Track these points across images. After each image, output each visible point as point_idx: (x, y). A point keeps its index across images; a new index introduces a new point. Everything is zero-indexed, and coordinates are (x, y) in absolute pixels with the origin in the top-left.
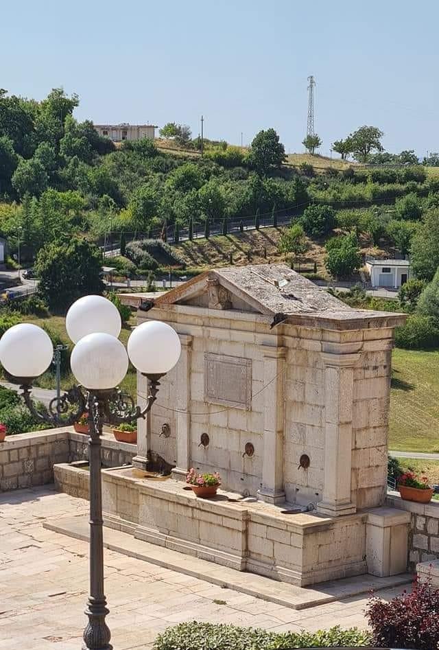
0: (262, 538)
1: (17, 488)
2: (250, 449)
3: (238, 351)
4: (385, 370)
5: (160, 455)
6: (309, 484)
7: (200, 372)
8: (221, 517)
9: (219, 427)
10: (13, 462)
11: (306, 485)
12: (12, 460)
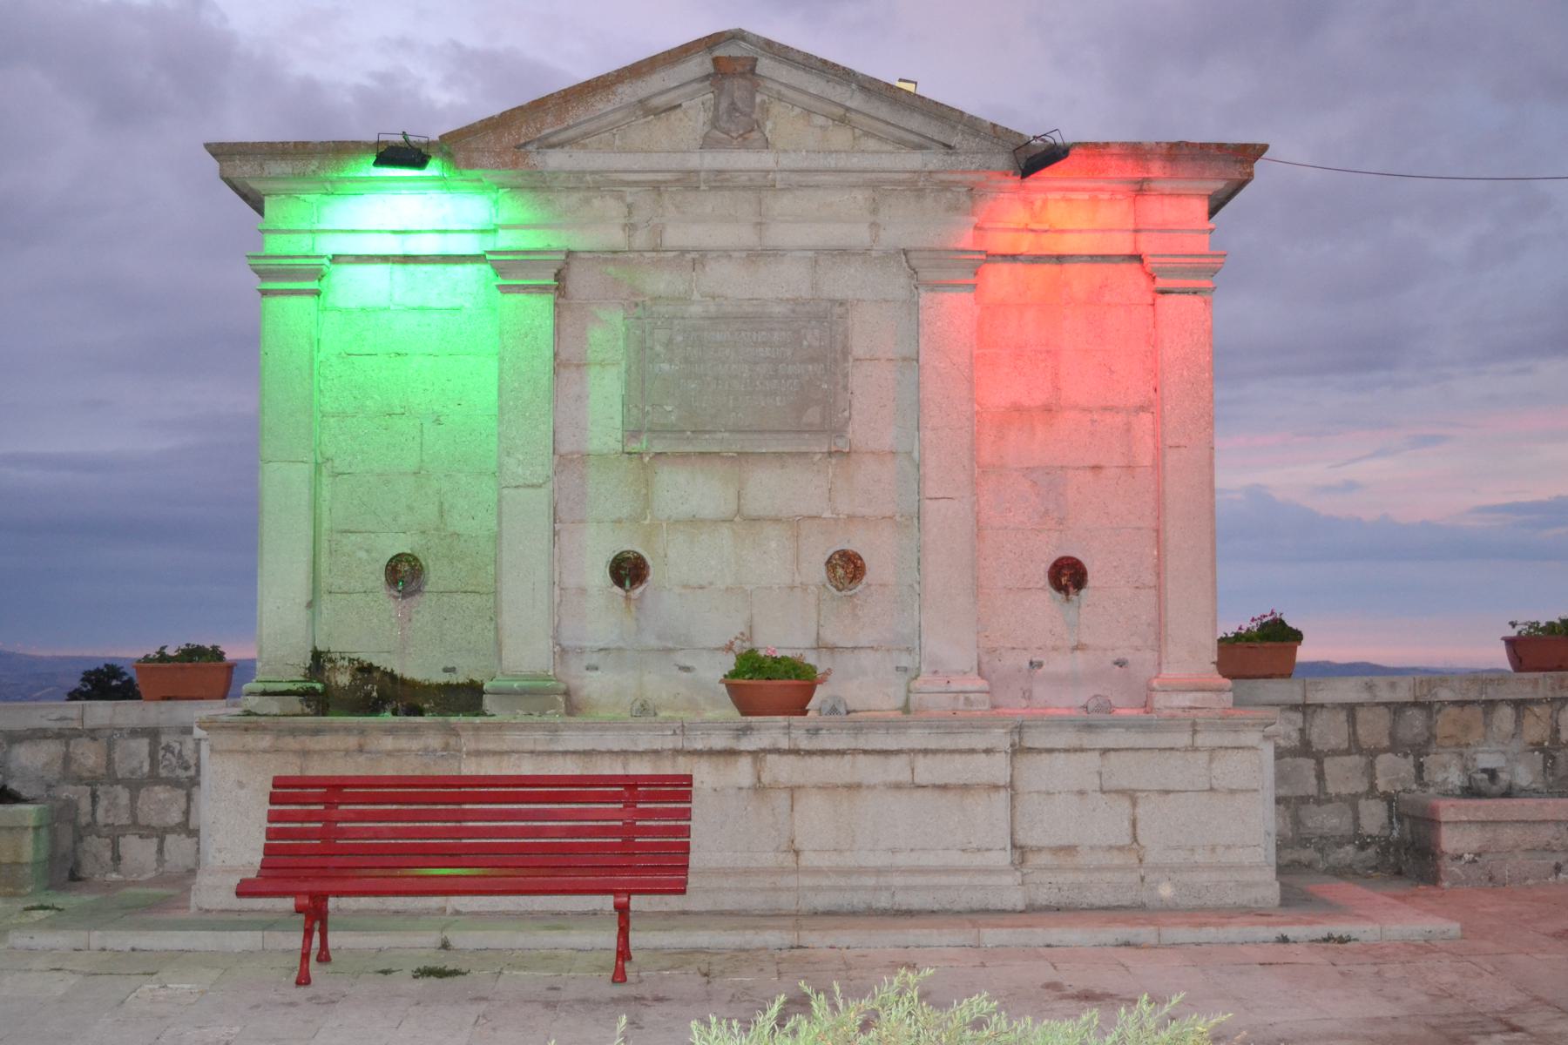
0: (1081, 793)
5: (367, 658)
6: (1085, 640)
9: (694, 522)
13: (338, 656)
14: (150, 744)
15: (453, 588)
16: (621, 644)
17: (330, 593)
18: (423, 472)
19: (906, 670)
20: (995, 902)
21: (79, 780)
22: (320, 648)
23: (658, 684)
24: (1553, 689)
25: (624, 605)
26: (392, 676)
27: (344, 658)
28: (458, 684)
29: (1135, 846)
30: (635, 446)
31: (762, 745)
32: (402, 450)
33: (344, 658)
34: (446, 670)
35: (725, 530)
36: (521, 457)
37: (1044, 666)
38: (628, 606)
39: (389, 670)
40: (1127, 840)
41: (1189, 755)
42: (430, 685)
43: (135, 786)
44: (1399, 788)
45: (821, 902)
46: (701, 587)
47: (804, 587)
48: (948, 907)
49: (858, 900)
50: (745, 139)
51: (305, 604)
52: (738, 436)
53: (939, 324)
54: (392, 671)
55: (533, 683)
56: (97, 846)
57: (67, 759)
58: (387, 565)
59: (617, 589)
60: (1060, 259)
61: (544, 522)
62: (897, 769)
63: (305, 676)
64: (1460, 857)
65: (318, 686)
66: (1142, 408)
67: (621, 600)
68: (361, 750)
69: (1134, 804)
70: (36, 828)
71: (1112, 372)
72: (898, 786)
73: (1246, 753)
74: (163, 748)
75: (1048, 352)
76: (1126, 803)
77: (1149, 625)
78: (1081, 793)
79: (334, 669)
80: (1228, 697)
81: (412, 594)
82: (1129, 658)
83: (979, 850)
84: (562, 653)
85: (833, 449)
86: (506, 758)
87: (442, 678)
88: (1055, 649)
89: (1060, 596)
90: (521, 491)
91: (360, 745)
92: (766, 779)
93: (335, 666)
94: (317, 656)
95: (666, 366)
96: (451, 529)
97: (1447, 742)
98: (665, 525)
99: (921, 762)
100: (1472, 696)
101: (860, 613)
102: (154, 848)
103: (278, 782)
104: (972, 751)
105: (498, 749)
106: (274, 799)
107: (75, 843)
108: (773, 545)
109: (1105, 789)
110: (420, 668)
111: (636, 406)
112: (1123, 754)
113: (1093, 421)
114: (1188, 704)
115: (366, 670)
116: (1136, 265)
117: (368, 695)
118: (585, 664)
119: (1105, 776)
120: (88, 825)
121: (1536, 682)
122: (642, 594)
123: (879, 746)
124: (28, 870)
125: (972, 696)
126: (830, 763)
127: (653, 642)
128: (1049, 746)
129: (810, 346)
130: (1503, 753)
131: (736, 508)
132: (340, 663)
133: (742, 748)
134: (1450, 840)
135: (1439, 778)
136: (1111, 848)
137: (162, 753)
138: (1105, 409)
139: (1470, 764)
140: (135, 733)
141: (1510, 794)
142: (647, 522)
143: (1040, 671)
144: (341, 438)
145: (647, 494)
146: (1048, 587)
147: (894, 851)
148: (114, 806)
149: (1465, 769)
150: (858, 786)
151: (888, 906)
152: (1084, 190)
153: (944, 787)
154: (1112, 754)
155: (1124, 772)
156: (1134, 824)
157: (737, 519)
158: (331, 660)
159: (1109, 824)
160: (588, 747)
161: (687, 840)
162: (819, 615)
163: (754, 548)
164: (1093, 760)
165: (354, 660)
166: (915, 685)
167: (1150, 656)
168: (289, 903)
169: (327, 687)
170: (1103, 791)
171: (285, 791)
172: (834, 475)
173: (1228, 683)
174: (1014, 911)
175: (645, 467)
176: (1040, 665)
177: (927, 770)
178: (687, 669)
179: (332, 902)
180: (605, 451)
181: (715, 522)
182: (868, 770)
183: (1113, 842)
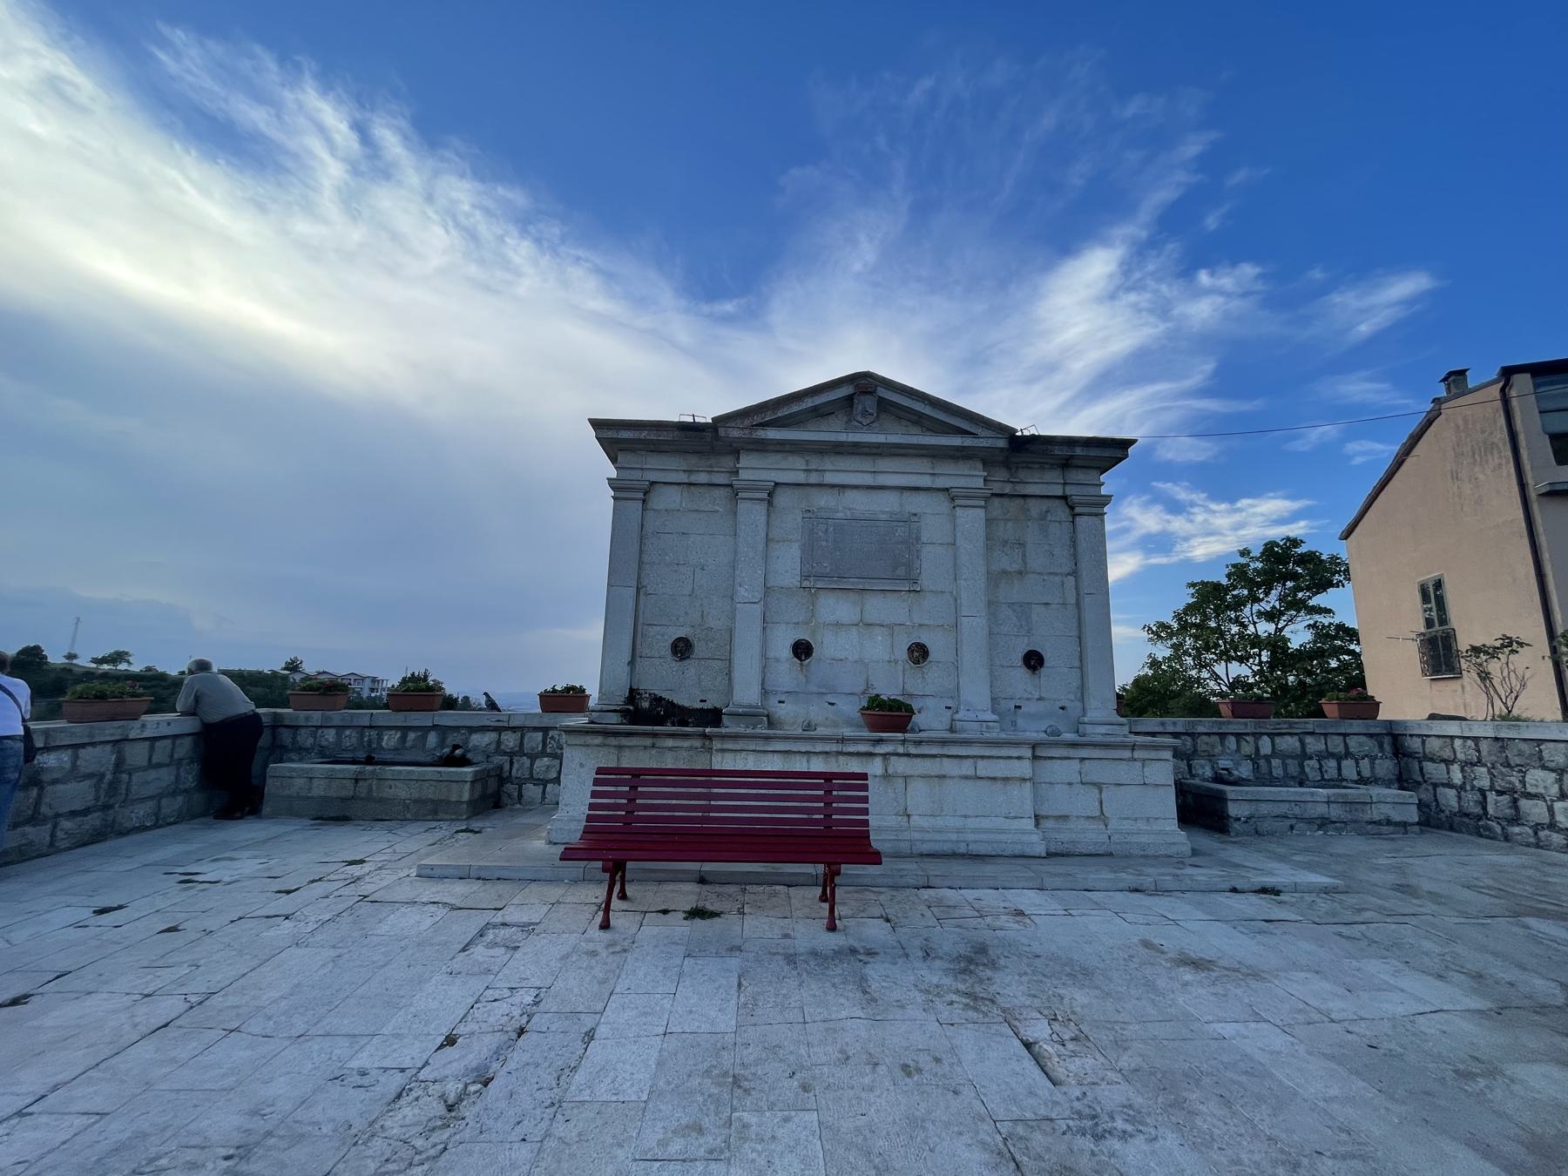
1: (156, 826)
2: (919, 653)
3: (885, 504)
4: (907, 511)
5: (659, 694)
6: (1043, 695)
7: (790, 541)
8: (970, 761)
10: (159, 766)
11: (1037, 696)
12: (155, 760)
19: (950, 708)
20: (1028, 851)
21: (505, 753)
22: (635, 687)
23: (816, 711)
24: (1255, 728)
26: (672, 703)
29: (1103, 817)
30: (806, 584)
31: (888, 751)
34: (701, 701)
38: (802, 669)
40: (1098, 814)
41: (1131, 763)
43: (533, 758)
44: (1180, 777)
45: (926, 848)
47: (896, 662)
48: (1000, 853)
49: (947, 848)
52: (862, 580)
56: (511, 788)
57: (499, 742)
59: (795, 660)
60: (1024, 496)
61: (759, 622)
62: (966, 768)
64: (1239, 819)
65: (631, 708)
68: (653, 746)
69: (1101, 792)
70: (472, 782)
72: (967, 778)
73: (1163, 763)
75: (1019, 544)
76: (1097, 791)
78: (1070, 784)
80: (1126, 729)
81: (684, 659)
83: (1016, 818)
84: (765, 693)
85: (912, 589)
86: (739, 754)
87: (699, 705)
92: (890, 771)
94: (632, 690)
95: (824, 543)
96: (707, 626)
97: (1203, 754)
99: (980, 763)
100: (1214, 731)
102: (541, 790)
103: (600, 771)
104: (1010, 758)
106: (596, 782)
107: (499, 787)
108: (880, 638)
109: (1084, 782)
110: (687, 698)
112: (1092, 761)
116: (1063, 502)
119: (1083, 775)
120: (507, 777)
121: (1246, 724)
122: (809, 662)
123: (955, 754)
124: (465, 806)
125: (990, 724)
126: (928, 763)
127: (814, 689)
128: (1050, 755)
129: (899, 535)
130: (1232, 760)
133: (877, 752)
134: (1233, 810)
135: (1200, 772)
136: (1088, 817)
137: (549, 740)
139: (1215, 766)
140: (536, 729)
141: (1517, 820)
143: (1020, 711)
147: (965, 817)
148: (521, 767)
149: (1213, 768)
150: (944, 777)
151: (965, 852)
152: (1038, 463)
153: (994, 779)
154: (1087, 761)
155: (1096, 771)
156: (1101, 803)
157: (861, 624)
158: (639, 694)
159: (1086, 802)
160: (787, 749)
161: (866, 817)
163: (1455, 476)
164: (1075, 765)
166: (957, 717)
167: (1079, 704)
168: (599, 864)
169: (636, 708)
170: (1082, 783)
171: (604, 775)
173: (1124, 720)
174: (1039, 857)
176: (1020, 707)
177: (984, 768)
178: (832, 704)
179: (629, 865)
180: (791, 586)
182: (949, 767)
183: (1089, 814)
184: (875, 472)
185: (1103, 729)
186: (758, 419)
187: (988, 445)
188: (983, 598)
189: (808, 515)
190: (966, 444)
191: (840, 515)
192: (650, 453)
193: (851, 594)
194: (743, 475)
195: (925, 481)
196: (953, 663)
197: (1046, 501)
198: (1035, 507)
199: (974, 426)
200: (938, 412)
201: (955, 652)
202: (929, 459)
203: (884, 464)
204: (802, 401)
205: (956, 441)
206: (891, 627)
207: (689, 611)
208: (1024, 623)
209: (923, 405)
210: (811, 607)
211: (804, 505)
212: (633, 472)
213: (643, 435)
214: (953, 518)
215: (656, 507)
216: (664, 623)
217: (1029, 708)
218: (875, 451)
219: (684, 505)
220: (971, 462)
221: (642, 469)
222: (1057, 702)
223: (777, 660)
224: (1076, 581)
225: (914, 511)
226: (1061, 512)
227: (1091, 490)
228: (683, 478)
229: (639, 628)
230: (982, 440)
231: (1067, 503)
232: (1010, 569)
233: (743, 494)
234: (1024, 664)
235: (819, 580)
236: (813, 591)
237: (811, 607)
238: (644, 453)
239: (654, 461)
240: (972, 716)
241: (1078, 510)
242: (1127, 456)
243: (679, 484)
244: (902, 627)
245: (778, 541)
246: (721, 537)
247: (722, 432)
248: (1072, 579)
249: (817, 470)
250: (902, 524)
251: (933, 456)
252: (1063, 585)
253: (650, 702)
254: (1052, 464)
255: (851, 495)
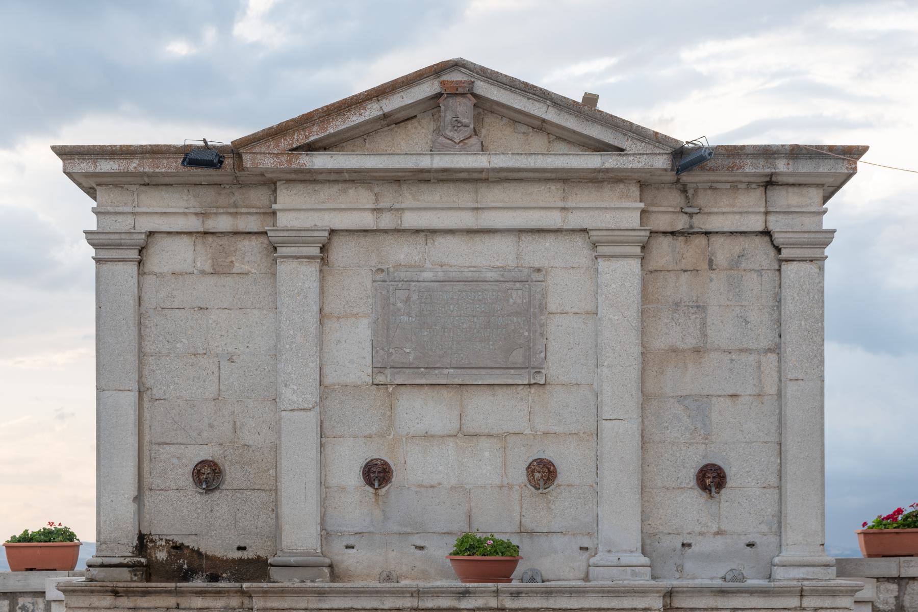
5: (179, 540)
6: (723, 528)
7: (356, 316)
9: (427, 437)
11: (714, 529)
13: (157, 538)
14: (10, 605)
15: (244, 486)
16: (372, 529)
17: (151, 490)
18: (220, 398)
25: (374, 500)
26: (198, 553)
27: (162, 539)
28: (248, 559)
30: (380, 379)
32: (204, 381)
33: (162, 539)
34: (240, 548)
35: (450, 442)
36: (295, 388)
37: (693, 547)
38: (377, 501)
39: (196, 549)
42: (227, 560)
46: (432, 487)
47: (510, 487)
50: (465, 144)
51: (132, 498)
52: (459, 371)
53: (613, 286)
54: (199, 549)
55: (302, 558)
58: (194, 470)
63: (133, 553)
66: (769, 350)
67: (372, 496)
71: (747, 322)
74: (20, 608)
75: (698, 307)
77: (773, 516)
79: (155, 547)
82: (757, 541)
85: (533, 381)
87: (237, 555)
88: (701, 534)
89: (705, 495)
90: (296, 413)
91: (178, 604)
93: (155, 545)
95: (405, 318)
98: (404, 439)
101: (553, 507)
105: (279, 607)
108: (487, 454)
111: (383, 349)
113: (732, 360)
114: (802, 576)
115: (178, 548)
116: (767, 239)
117: (181, 567)
118: (345, 543)
127: (396, 528)
131: (458, 426)
132: (158, 543)
138: (741, 350)
142: (391, 437)
144: (157, 372)
145: (391, 416)
146: (696, 487)
158: (152, 541)
162: (521, 508)
165: (169, 541)
172: (534, 402)
175: (390, 395)
178: (421, 548)
180: (359, 383)
181: (442, 437)
184: (477, 209)
185: (800, 573)
186: (299, 139)
187: (640, 166)
188: (634, 392)
189: (380, 276)
190: (607, 165)
191: (427, 275)
192: (143, 188)
193: (444, 392)
194: (284, 220)
195: (553, 219)
196: (592, 486)
197: (741, 239)
198: (723, 250)
199: (621, 136)
200: (567, 116)
201: (594, 469)
202: (560, 185)
203: (493, 195)
204: (364, 108)
205: (593, 161)
206: (503, 437)
207: (215, 423)
208: (699, 425)
209: (545, 108)
210: (389, 413)
211: (374, 261)
212: (120, 218)
213: (133, 165)
214: (594, 271)
215: (156, 269)
216: (180, 440)
217: (701, 546)
218: (476, 176)
219: (199, 265)
220: (622, 186)
221: (134, 214)
222: (743, 537)
223: (342, 489)
224: (779, 361)
225: (537, 265)
226: (761, 252)
227: (808, 223)
228: (194, 224)
229: (146, 448)
230: (631, 158)
231: (772, 241)
232: (680, 345)
233: (284, 249)
234: (698, 485)
235: (397, 373)
236: (390, 389)
237: (389, 413)
238: (133, 188)
239: (152, 201)
240: (613, 559)
241: (785, 253)
242: (854, 171)
243: (190, 233)
244: (521, 436)
245: (338, 318)
246: (256, 312)
247: (248, 161)
248: (773, 357)
249: (390, 209)
250: (518, 285)
251: (565, 181)
252: (759, 367)
253: (169, 552)
254: (749, 183)
255: (443, 244)
